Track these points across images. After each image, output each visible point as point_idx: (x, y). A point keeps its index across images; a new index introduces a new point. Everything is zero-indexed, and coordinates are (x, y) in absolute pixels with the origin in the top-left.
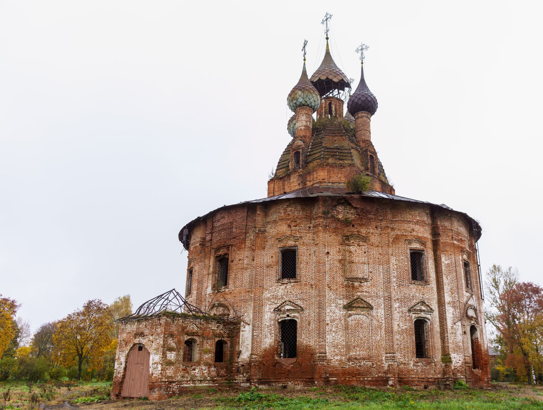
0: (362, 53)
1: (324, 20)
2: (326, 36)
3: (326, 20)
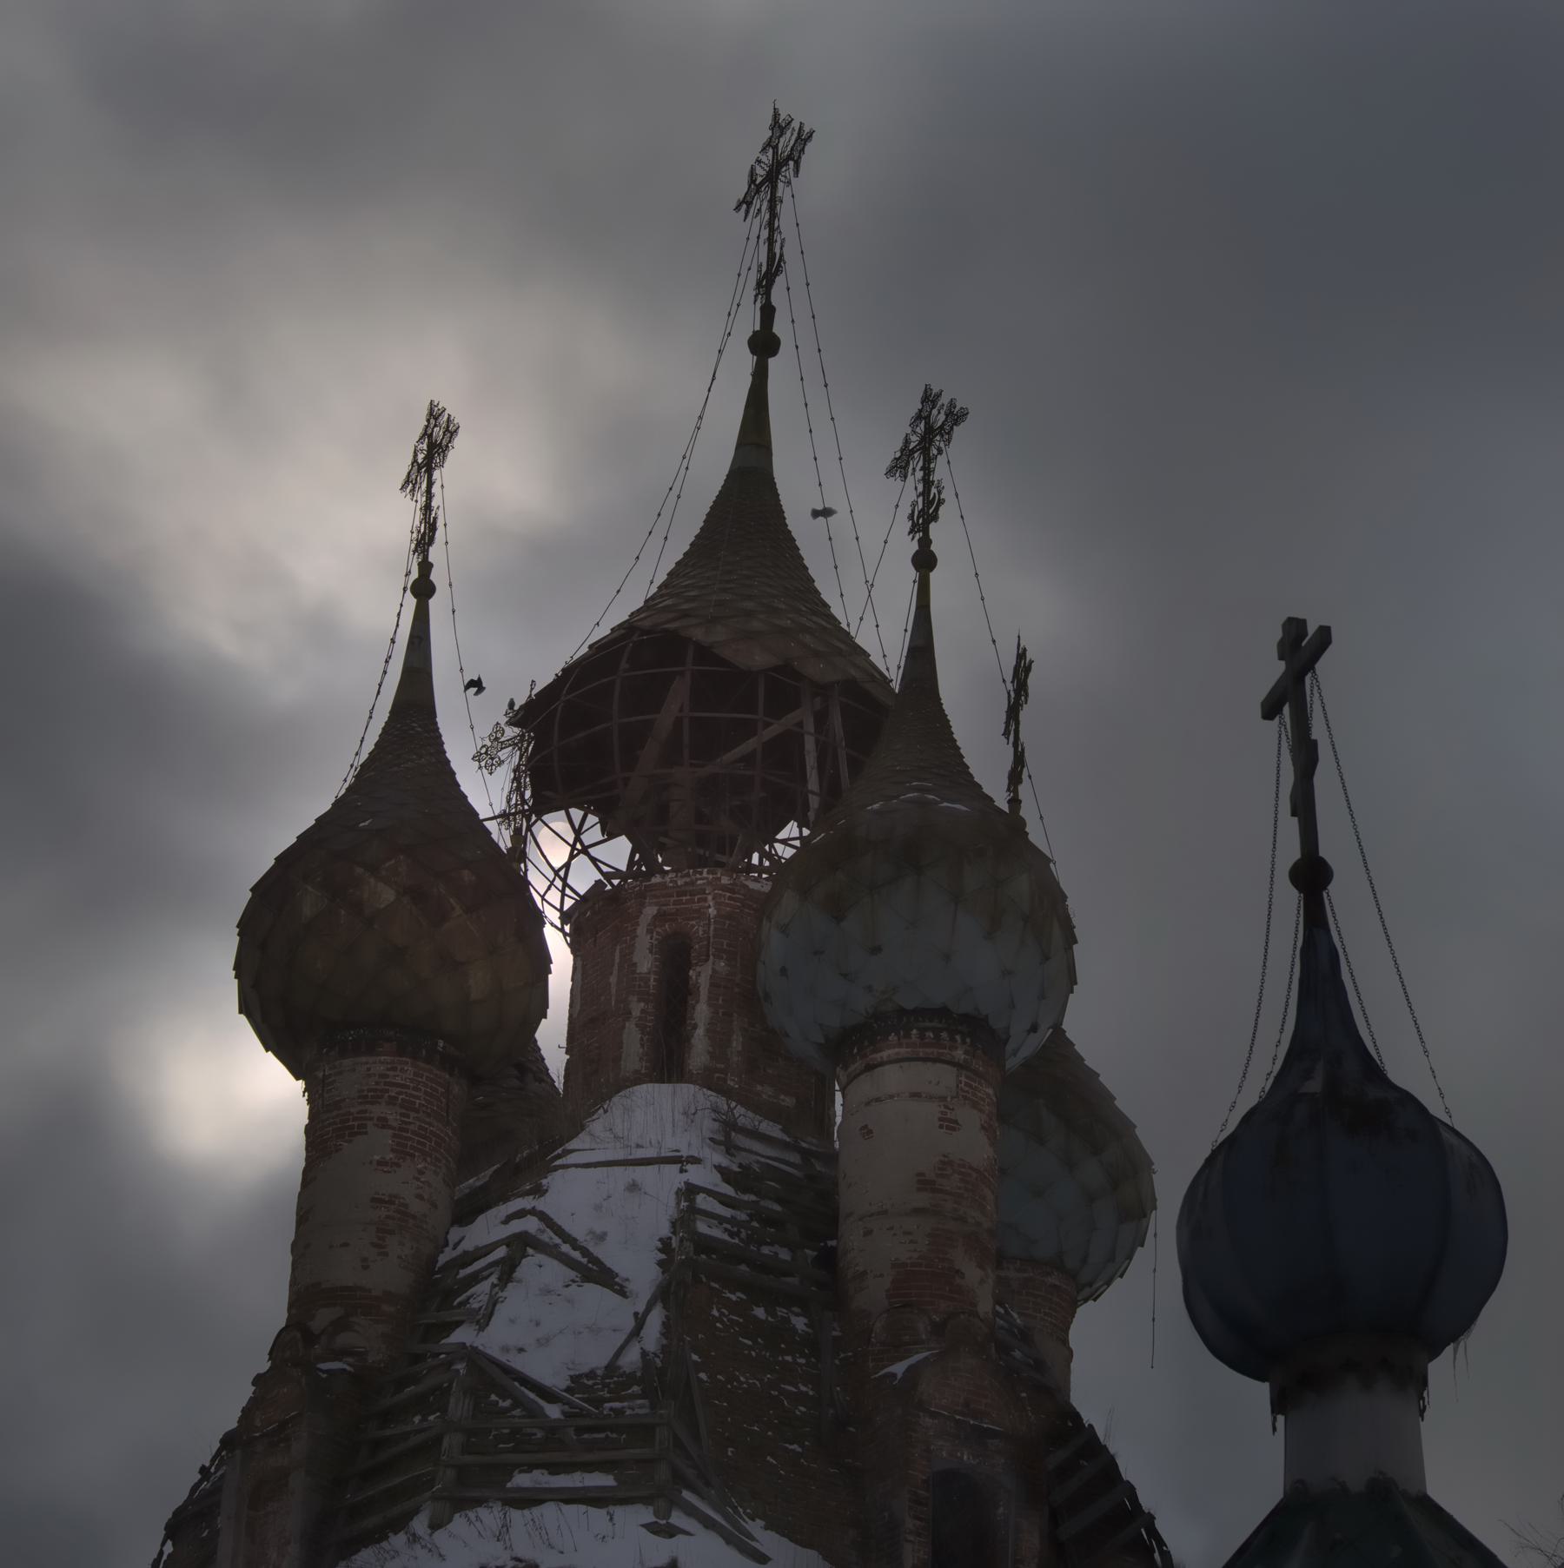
3: (772, 177)
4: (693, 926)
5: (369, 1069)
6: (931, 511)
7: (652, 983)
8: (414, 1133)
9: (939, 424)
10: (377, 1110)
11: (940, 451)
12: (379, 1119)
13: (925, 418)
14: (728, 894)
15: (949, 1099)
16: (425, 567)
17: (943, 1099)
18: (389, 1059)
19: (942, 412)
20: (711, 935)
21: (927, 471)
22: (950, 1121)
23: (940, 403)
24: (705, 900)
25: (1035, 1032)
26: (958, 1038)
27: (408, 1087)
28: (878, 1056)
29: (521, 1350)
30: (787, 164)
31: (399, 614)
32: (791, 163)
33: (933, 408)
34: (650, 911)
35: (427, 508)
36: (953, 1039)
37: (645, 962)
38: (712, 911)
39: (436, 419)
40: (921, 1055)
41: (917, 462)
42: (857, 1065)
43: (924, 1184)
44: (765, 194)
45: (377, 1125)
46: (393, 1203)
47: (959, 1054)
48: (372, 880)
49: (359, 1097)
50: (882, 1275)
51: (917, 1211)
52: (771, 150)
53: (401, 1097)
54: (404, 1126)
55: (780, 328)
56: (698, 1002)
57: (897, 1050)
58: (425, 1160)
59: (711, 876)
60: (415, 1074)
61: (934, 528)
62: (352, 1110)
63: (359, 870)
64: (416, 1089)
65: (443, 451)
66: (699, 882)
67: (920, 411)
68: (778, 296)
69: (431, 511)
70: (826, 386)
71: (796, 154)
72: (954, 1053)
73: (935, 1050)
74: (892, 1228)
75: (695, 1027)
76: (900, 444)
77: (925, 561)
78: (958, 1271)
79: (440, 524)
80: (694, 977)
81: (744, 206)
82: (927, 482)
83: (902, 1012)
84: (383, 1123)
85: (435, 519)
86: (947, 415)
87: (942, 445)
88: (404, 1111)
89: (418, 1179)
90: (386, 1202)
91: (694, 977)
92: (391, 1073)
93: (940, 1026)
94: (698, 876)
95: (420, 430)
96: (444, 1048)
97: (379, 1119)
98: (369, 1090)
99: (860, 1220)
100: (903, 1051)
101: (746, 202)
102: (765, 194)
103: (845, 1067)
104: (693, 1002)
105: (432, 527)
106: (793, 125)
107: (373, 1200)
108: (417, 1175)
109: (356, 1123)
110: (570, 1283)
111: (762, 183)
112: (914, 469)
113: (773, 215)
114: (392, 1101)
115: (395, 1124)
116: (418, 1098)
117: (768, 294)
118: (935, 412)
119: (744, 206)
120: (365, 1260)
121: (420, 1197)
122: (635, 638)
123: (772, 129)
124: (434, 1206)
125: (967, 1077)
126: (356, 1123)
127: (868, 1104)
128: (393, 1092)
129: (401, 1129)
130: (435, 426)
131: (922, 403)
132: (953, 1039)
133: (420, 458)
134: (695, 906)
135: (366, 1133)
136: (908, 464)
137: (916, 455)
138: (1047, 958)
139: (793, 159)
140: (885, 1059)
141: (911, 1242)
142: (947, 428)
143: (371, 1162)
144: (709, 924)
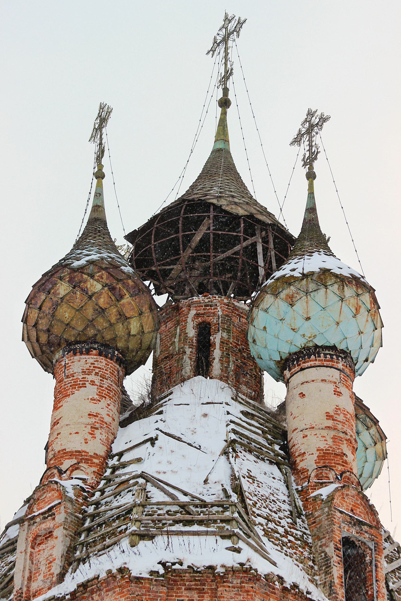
0: (226, 49)
1: (219, 39)
2: (220, 95)
3: (225, 40)
4: (211, 319)
5: (86, 361)
6: (313, 157)
7: (194, 341)
8: (106, 388)
9: (316, 122)
10: (90, 378)
11: (317, 133)
12: (91, 381)
13: (309, 122)
14: (226, 307)
15: (337, 383)
16: (100, 166)
17: (335, 383)
18: (95, 357)
19: (318, 118)
20: (220, 322)
21: (310, 141)
22: (339, 392)
23: (316, 115)
24: (217, 309)
25: (367, 362)
26: (340, 358)
27: (103, 369)
28: (306, 365)
29: (165, 473)
30: (233, 33)
31: (92, 183)
32: (235, 33)
33: (313, 117)
34: (193, 312)
35: (101, 144)
36: (338, 359)
37: (192, 332)
38: (220, 313)
39: (103, 109)
40: (325, 365)
41: (306, 138)
42: (297, 368)
43: (329, 416)
44: (222, 48)
45: (89, 384)
46: (98, 417)
47: (340, 366)
48: (91, 280)
49: (82, 372)
50: (313, 454)
51: (328, 428)
52: (224, 29)
53: (100, 373)
54: (101, 385)
55: (231, 96)
56: (215, 349)
57: (314, 362)
58: (110, 400)
59: (219, 299)
60: (106, 364)
61: (316, 164)
62: (79, 377)
63: (85, 276)
64: (106, 370)
65: (106, 120)
66: (215, 301)
67: (306, 119)
68: (229, 84)
69: (102, 145)
70: (254, 117)
71: (238, 30)
72: (338, 365)
73: (331, 363)
74: (316, 435)
75: (214, 359)
76: (297, 132)
77: (311, 176)
78: (344, 454)
79: (106, 149)
80: (213, 339)
81: (211, 52)
82: (311, 146)
83: (316, 346)
84: (93, 383)
85: (104, 147)
86: (320, 119)
87: (318, 131)
88: (101, 379)
89: (108, 408)
90: (95, 416)
91: (213, 339)
92: (96, 363)
93: (333, 353)
94: (214, 299)
95: (96, 115)
96: (117, 354)
97: (91, 381)
98: (87, 369)
99: (302, 431)
100: (317, 363)
101: (213, 50)
102: (222, 48)
103: (290, 370)
104: (213, 349)
105: (103, 152)
106: (235, 18)
107: (89, 415)
108: (107, 406)
109: (81, 383)
110: (229, 423)
111: (220, 42)
112: (304, 141)
113: (226, 54)
114: (97, 374)
115: (98, 384)
116: (107, 374)
117: (225, 84)
118: (314, 118)
119: (211, 52)
120: (86, 439)
121: (108, 415)
122: (186, 203)
123: (225, 21)
124: (114, 420)
125: (343, 375)
126: (81, 383)
127: (302, 384)
128: (97, 370)
129: (100, 386)
130: (103, 111)
131: (307, 116)
132: (338, 359)
133: (97, 126)
134: (212, 311)
135: (86, 387)
136: (301, 139)
137: (305, 136)
138: (376, 329)
139: (236, 31)
140: (309, 366)
141: (325, 440)
142: (320, 124)
143: (88, 399)
144: (219, 318)
